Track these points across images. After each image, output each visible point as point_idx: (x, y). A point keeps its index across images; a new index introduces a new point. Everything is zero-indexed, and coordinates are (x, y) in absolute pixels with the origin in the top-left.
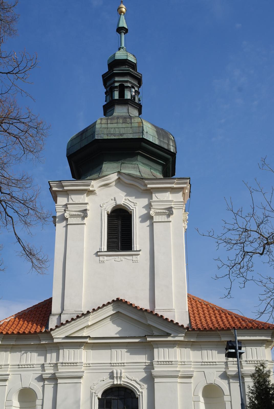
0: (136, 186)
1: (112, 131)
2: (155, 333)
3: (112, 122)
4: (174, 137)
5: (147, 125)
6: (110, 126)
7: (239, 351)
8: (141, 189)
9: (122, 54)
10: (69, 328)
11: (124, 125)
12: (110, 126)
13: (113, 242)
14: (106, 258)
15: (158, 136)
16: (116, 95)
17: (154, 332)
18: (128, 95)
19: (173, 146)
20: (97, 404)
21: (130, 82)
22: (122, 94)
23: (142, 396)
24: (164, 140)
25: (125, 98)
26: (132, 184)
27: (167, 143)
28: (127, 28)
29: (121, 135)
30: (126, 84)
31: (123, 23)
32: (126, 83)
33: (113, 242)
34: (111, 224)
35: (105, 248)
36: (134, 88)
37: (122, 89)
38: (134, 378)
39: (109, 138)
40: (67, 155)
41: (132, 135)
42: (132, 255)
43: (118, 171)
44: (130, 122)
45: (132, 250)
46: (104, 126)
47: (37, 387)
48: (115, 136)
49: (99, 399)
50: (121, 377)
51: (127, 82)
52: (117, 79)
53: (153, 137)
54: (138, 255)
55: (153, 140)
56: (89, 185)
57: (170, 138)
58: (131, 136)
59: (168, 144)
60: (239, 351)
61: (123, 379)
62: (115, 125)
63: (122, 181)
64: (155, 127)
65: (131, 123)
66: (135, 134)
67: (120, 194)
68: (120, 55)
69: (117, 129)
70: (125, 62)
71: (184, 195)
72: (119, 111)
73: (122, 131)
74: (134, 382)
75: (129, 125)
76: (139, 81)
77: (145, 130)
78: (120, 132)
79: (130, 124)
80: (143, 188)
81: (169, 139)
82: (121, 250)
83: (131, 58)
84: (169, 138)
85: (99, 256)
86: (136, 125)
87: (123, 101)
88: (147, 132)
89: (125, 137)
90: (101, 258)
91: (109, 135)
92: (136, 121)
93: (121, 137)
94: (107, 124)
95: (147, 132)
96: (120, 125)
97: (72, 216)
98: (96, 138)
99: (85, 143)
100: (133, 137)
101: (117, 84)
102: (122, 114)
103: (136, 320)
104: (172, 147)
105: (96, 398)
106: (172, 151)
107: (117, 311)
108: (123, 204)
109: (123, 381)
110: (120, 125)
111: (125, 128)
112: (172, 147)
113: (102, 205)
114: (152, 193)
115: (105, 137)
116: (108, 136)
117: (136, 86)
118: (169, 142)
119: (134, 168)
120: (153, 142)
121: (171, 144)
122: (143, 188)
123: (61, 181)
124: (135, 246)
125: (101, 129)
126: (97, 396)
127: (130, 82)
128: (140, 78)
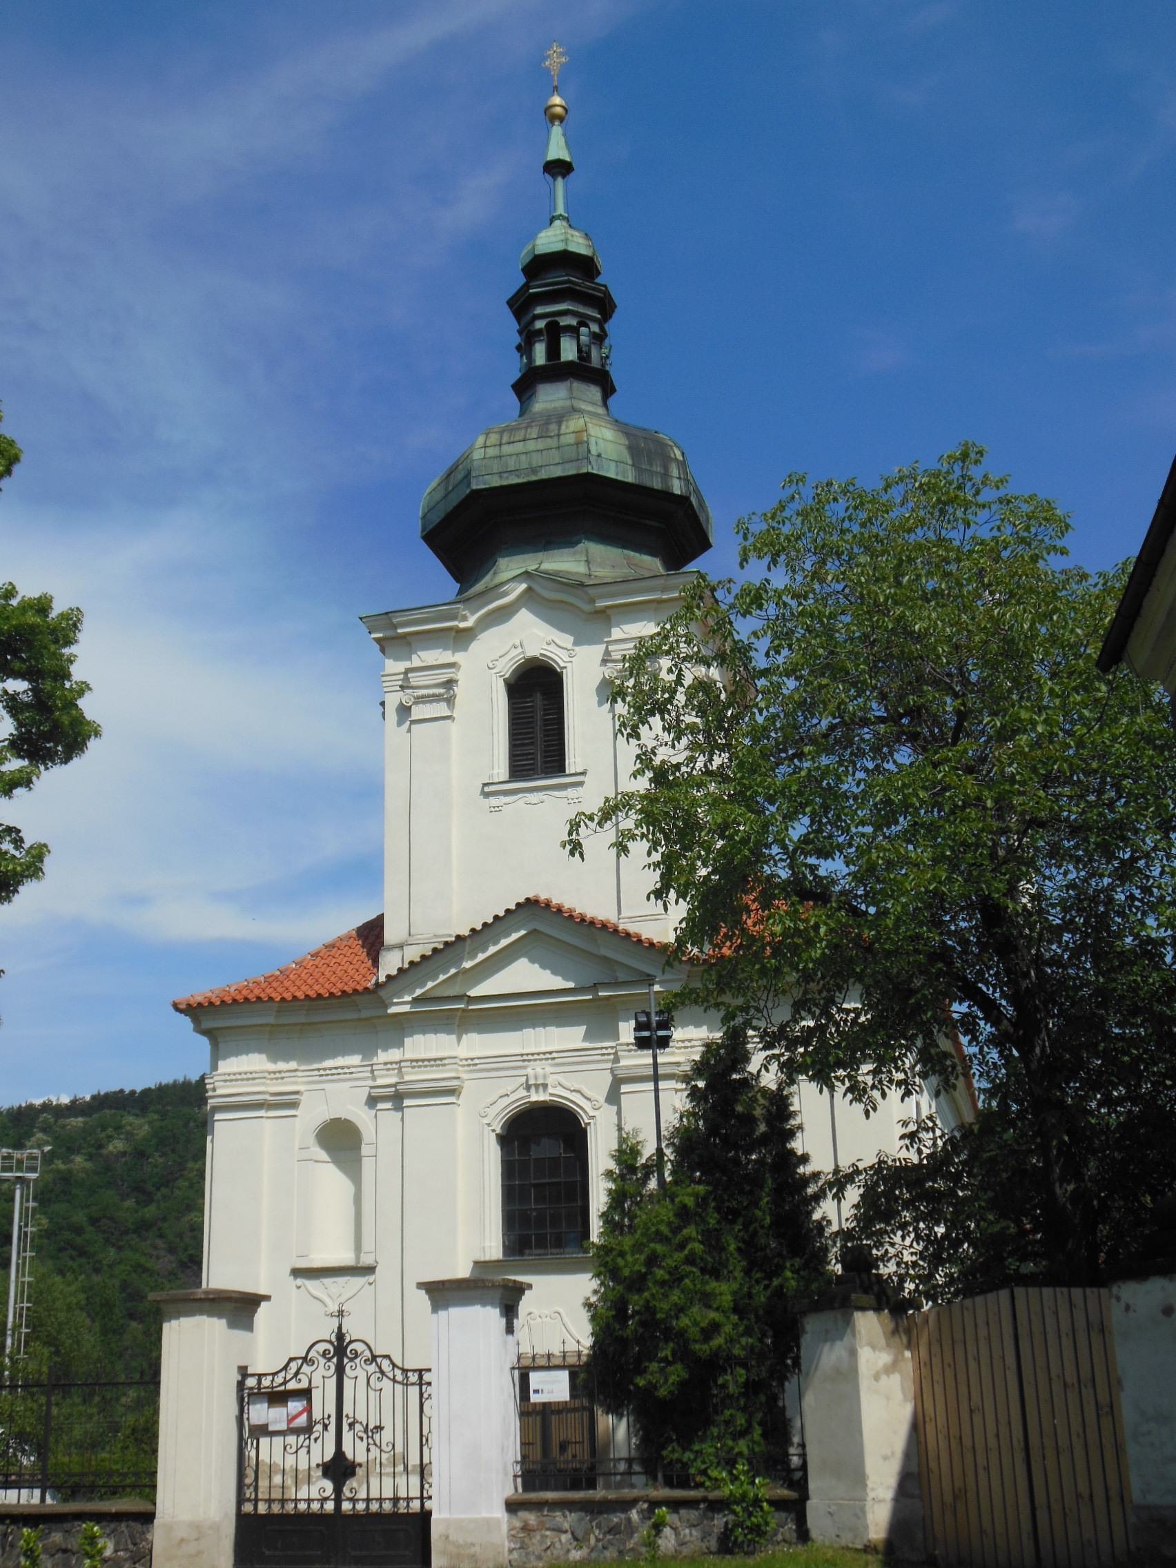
0: (572, 605)
1: (512, 464)
2: (622, 977)
3: (512, 440)
4: (683, 454)
5: (600, 435)
6: (507, 449)
8: (583, 611)
9: (554, 239)
10: (346, 1021)
11: (541, 444)
12: (507, 449)
13: (523, 755)
14: (503, 799)
15: (633, 459)
16: (540, 354)
17: (618, 974)
18: (568, 351)
19: (679, 478)
22: (553, 351)
23: (595, 1124)
24: (651, 465)
25: (562, 360)
26: (561, 602)
27: (662, 471)
28: (568, 159)
29: (534, 471)
30: (564, 321)
31: (557, 149)
32: (564, 318)
33: (523, 755)
34: (521, 708)
35: (500, 768)
36: (587, 326)
37: (554, 334)
38: (576, 1087)
39: (505, 483)
40: (423, 530)
41: (560, 467)
43: (523, 570)
44: (556, 432)
45: (564, 771)
46: (491, 452)
47: (361, 1116)
48: (518, 476)
50: (545, 1086)
52: (539, 310)
53: (617, 466)
54: (581, 784)
55: (617, 474)
57: (673, 456)
58: (558, 472)
59: (666, 475)
61: (551, 1090)
62: (519, 447)
63: (539, 595)
64: (627, 434)
65: (559, 435)
66: (567, 466)
67: (535, 631)
68: (550, 240)
69: (523, 457)
70: (563, 259)
72: (550, 397)
73: (537, 460)
74: (578, 1095)
75: (552, 443)
76: (605, 306)
77: (594, 451)
78: (530, 463)
79: (556, 439)
80: (587, 608)
81: (666, 460)
82: (542, 772)
83: (579, 245)
84: (670, 457)
86: (570, 439)
87: (556, 371)
88: (599, 456)
89: (543, 475)
90: (493, 801)
91: (505, 475)
92: (571, 429)
93: (534, 478)
94: (500, 445)
95: (599, 456)
96: (531, 445)
97: (421, 700)
98: (474, 487)
99: (455, 500)
100: (562, 474)
101: (540, 324)
102: (553, 405)
103: (575, 947)
106: (677, 491)
107: (532, 926)
108: (541, 654)
109: (551, 1095)
110: (531, 445)
111: (544, 452)
113: (491, 666)
115: (496, 482)
116: (501, 477)
117: (594, 319)
118: (666, 468)
120: (620, 478)
122: (587, 608)
123: (387, 613)
124: (572, 760)
125: (484, 462)
126: (493, 1131)
128: (602, 295)
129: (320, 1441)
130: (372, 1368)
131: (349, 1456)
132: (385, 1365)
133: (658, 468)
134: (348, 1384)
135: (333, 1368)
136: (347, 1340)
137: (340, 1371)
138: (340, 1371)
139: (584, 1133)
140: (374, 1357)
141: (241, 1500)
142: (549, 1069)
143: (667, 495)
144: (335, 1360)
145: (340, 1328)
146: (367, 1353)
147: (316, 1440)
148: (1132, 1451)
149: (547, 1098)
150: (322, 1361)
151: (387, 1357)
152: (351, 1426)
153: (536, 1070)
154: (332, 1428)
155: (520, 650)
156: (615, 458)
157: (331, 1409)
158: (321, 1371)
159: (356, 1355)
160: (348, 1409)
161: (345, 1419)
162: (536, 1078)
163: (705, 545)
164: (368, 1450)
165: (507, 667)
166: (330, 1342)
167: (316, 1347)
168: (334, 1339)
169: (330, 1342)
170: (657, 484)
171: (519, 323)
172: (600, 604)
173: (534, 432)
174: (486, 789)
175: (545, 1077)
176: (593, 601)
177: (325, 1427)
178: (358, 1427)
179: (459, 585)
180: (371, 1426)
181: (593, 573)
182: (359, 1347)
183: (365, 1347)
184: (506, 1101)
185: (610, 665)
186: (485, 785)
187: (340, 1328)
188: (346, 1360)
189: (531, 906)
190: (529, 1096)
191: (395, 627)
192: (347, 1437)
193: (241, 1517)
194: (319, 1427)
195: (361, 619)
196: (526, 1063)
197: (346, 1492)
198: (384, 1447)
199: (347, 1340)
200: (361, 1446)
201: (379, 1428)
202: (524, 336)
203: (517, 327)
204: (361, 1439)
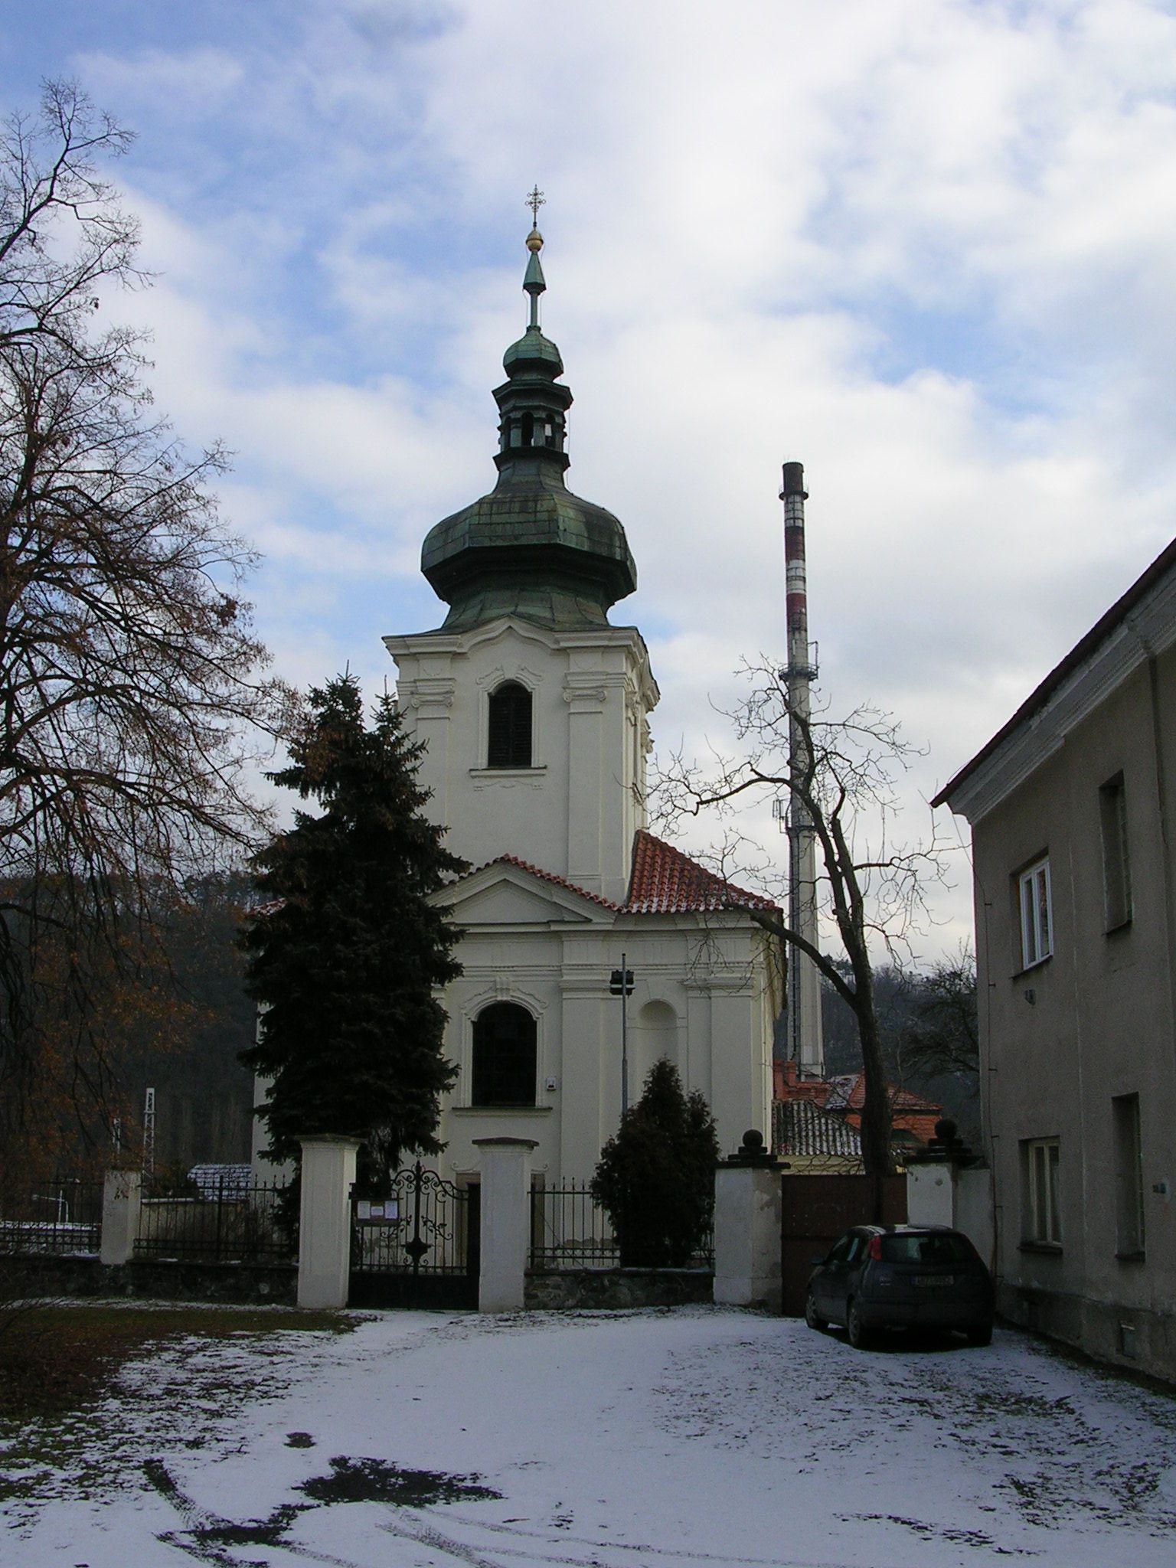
6: (496, 519)
7: (629, 986)
19: (620, 547)
20: (814, 1027)
21: (544, 408)
26: (529, 638)
29: (516, 538)
35: (483, 760)
39: (493, 544)
42: (530, 776)
45: (530, 764)
49: (473, 1022)
51: (537, 408)
55: (577, 545)
56: (93, 1410)
59: (611, 546)
60: (629, 986)
62: (505, 518)
65: (536, 512)
71: (630, 656)
75: (531, 517)
85: (473, 777)
86: (544, 516)
88: (565, 530)
89: (523, 541)
90: (477, 782)
92: (545, 508)
93: (516, 543)
94: (491, 514)
96: (514, 518)
104: (618, 550)
105: (469, 1023)
106: (618, 558)
109: (512, 996)
110: (514, 518)
112: (618, 550)
114: (569, 655)
115: (487, 543)
116: (491, 540)
118: (611, 539)
119: (542, 600)
121: (618, 544)
122: (555, 646)
127: (544, 408)
129: (404, 1232)
130: (439, 1188)
131: (423, 1240)
132: (448, 1187)
133: (605, 540)
134: (423, 1198)
135: (413, 1187)
136: (423, 1170)
137: (418, 1189)
138: (418, 1189)
139: (534, 1024)
140: (441, 1182)
141: (352, 1263)
142: (511, 979)
143: (611, 560)
144: (415, 1183)
145: (418, 1163)
146: (436, 1179)
147: (402, 1230)
148: (780, 1184)
149: (509, 999)
150: (406, 1183)
151: (449, 1182)
152: (425, 1224)
153: (502, 978)
154: (413, 1223)
155: (501, 673)
156: (575, 532)
157: (412, 1212)
158: (405, 1188)
159: (428, 1180)
160: (422, 1212)
161: (421, 1219)
162: (502, 984)
163: (569, 466)
164: (436, 1238)
165: (491, 684)
166: (412, 1172)
167: (402, 1174)
168: (414, 1169)
169: (412, 1172)
170: (604, 552)
171: (500, 408)
172: (563, 644)
173: (517, 507)
174: (474, 773)
175: (508, 984)
176: (557, 641)
177: (408, 1223)
178: (429, 1224)
179: (446, 608)
180: (438, 1224)
181: (556, 619)
182: (431, 1175)
183: (434, 1175)
184: (480, 998)
185: (568, 691)
186: (471, 770)
187: (418, 1163)
188: (422, 1183)
189: (505, 861)
190: (496, 996)
191: (408, 647)
192: (422, 1229)
193: (353, 1276)
194: (404, 1223)
195: (383, 638)
196: (495, 973)
197: (422, 1262)
198: (446, 1236)
199: (423, 1170)
200: (431, 1235)
201: (443, 1225)
202: (504, 419)
203: (499, 412)
204: (432, 1231)
